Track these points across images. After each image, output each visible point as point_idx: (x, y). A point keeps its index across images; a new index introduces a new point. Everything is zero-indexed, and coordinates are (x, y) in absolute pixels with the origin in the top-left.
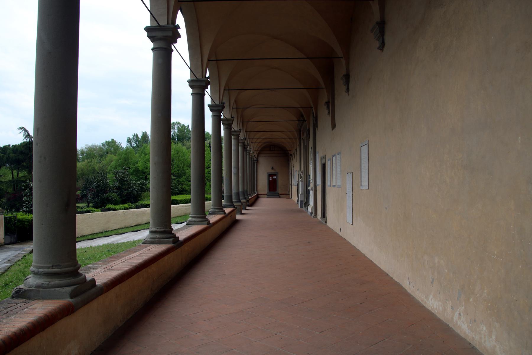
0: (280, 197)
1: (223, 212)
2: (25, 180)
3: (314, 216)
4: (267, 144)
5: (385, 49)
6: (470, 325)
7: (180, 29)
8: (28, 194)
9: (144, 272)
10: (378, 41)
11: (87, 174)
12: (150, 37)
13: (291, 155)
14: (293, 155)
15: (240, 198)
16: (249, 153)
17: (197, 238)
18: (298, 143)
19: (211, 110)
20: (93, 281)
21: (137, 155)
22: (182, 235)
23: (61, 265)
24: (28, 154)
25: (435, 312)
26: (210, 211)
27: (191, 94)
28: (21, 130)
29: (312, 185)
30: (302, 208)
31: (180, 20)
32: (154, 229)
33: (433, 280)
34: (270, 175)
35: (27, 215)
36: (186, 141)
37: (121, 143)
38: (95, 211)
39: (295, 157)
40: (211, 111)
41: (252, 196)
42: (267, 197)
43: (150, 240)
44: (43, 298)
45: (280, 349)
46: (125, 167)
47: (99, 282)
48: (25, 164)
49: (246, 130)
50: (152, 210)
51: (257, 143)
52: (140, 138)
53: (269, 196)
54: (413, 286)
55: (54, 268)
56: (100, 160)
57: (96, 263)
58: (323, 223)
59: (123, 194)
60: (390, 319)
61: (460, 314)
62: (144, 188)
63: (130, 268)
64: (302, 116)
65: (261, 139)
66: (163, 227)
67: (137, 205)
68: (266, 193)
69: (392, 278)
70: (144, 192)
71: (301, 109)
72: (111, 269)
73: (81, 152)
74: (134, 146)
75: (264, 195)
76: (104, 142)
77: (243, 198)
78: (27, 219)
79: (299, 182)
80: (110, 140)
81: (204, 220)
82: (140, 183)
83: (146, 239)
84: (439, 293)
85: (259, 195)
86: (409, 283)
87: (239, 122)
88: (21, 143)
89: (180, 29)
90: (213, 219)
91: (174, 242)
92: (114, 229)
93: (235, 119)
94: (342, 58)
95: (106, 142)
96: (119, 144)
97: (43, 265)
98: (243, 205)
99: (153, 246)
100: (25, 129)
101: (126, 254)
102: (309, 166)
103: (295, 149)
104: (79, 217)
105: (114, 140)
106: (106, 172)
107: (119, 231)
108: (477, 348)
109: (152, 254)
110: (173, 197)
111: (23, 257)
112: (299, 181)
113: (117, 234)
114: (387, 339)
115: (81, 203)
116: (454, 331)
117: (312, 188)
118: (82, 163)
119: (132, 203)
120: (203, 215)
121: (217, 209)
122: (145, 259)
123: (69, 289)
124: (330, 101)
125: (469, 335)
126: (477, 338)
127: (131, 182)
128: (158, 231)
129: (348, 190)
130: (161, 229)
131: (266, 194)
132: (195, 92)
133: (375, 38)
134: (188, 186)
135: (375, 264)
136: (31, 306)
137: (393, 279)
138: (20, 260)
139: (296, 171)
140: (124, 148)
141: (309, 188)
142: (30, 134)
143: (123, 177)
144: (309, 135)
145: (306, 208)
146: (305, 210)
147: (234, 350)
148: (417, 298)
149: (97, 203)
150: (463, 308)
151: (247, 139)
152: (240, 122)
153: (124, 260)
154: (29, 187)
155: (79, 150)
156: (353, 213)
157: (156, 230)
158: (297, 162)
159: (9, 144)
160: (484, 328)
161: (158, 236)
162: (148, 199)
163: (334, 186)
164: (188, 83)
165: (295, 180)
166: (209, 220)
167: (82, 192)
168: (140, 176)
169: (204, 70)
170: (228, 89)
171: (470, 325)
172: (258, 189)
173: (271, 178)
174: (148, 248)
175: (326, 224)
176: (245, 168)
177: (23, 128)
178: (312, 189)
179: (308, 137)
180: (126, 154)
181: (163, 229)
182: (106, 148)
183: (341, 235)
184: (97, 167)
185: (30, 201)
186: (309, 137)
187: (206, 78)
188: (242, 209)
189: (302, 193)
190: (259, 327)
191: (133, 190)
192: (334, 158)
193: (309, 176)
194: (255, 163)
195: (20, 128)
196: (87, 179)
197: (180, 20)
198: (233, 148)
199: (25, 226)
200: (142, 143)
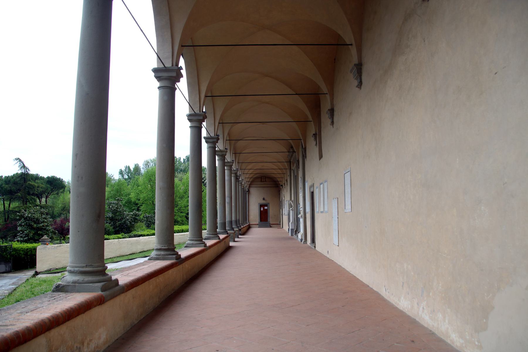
0: (271, 227)
1: (218, 238)
2: (18, 210)
4: (258, 175)
5: (362, 87)
6: (431, 315)
8: (23, 224)
9: (153, 281)
10: (357, 80)
12: (156, 77)
13: (282, 186)
14: (284, 185)
15: (233, 227)
16: (241, 183)
18: (289, 174)
19: (207, 142)
20: (117, 281)
21: (129, 186)
23: (93, 265)
24: (23, 185)
25: (406, 311)
26: (206, 237)
27: (190, 127)
28: (17, 161)
29: (302, 213)
30: (293, 236)
31: (182, 63)
33: (403, 283)
34: (261, 206)
35: (23, 244)
36: (178, 173)
37: (112, 175)
39: (286, 187)
42: (258, 227)
43: (155, 256)
44: (78, 291)
46: (118, 198)
47: (121, 282)
48: (19, 194)
49: (238, 161)
51: (249, 179)
52: (132, 170)
53: (260, 226)
54: (389, 292)
55: (88, 267)
58: (312, 248)
59: (116, 225)
61: (423, 308)
62: (137, 219)
64: (292, 147)
65: (253, 170)
66: (167, 245)
67: (130, 236)
68: (258, 223)
69: (372, 289)
70: (137, 223)
74: (126, 178)
75: (255, 225)
78: (22, 248)
79: (289, 211)
82: (133, 214)
84: (408, 294)
86: (386, 290)
87: (232, 154)
88: (14, 175)
90: (209, 243)
93: (228, 151)
94: (327, 94)
96: (111, 176)
97: (78, 265)
98: (236, 233)
99: (158, 261)
100: (20, 161)
102: (299, 194)
103: (286, 179)
107: (115, 260)
110: (176, 228)
111: (26, 280)
112: (290, 210)
117: (302, 215)
119: (125, 234)
120: (200, 238)
123: (100, 285)
124: (317, 133)
127: (125, 213)
128: (163, 249)
129: (334, 214)
131: (257, 224)
134: (180, 217)
135: (358, 279)
136: (71, 296)
138: (24, 283)
139: (287, 201)
140: (116, 180)
141: (299, 216)
142: (25, 165)
143: (117, 208)
144: (299, 165)
145: (296, 235)
146: (295, 237)
147: (234, 338)
150: (426, 302)
151: (239, 170)
152: (233, 153)
154: (24, 217)
157: (160, 247)
158: (288, 192)
159: (2, 175)
160: (441, 315)
162: (141, 230)
163: (322, 212)
164: (187, 117)
165: (285, 210)
168: (132, 207)
169: (202, 106)
170: (222, 123)
171: (431, 315)
172: (250, 219)
173: (262, 208)
175: (315, 249)
176: (237, 198)
177: (18, 159)
178: (302, 217)
179: (298, 167)
180: (118, 186)
183: (328, 257)
185: (24, 231)
186: (299, 168)
189: (292, 222)
191: (126, 221)
192: (322, 186)
193: (299, 205)
194: (246, 193)
195: (16, 159)
197: (182, 63)
198: (227, 178)
199: (21, 255)
200: (134, 175)
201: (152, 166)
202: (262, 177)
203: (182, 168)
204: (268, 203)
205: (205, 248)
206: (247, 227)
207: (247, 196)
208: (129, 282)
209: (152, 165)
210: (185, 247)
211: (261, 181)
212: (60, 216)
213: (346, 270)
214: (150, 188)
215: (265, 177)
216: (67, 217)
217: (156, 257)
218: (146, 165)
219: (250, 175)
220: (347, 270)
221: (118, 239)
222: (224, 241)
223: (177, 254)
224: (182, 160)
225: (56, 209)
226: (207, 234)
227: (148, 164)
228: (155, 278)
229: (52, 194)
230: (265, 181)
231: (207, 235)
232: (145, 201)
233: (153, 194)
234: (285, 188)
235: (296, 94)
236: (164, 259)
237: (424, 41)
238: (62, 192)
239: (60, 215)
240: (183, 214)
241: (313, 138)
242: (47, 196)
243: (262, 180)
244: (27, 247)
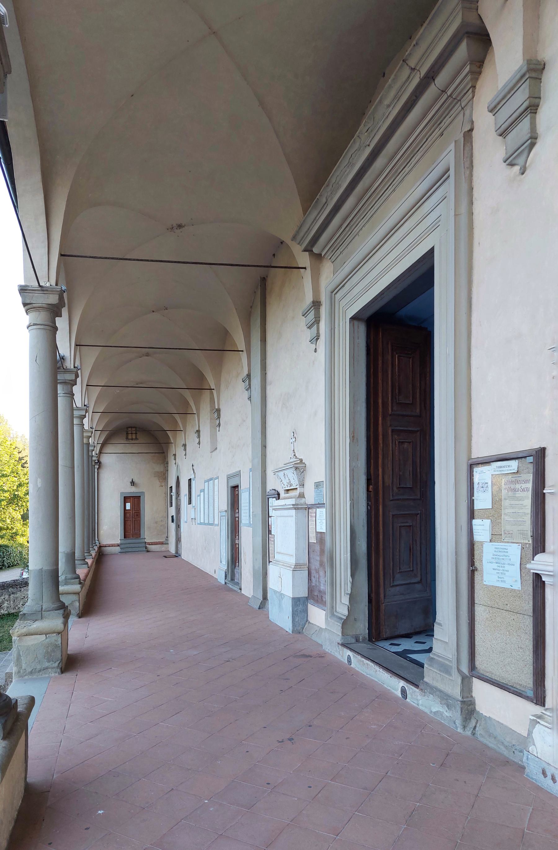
68: (119, 542)
202: (130, 429)
243: (130, 437)
244: (48, 647)
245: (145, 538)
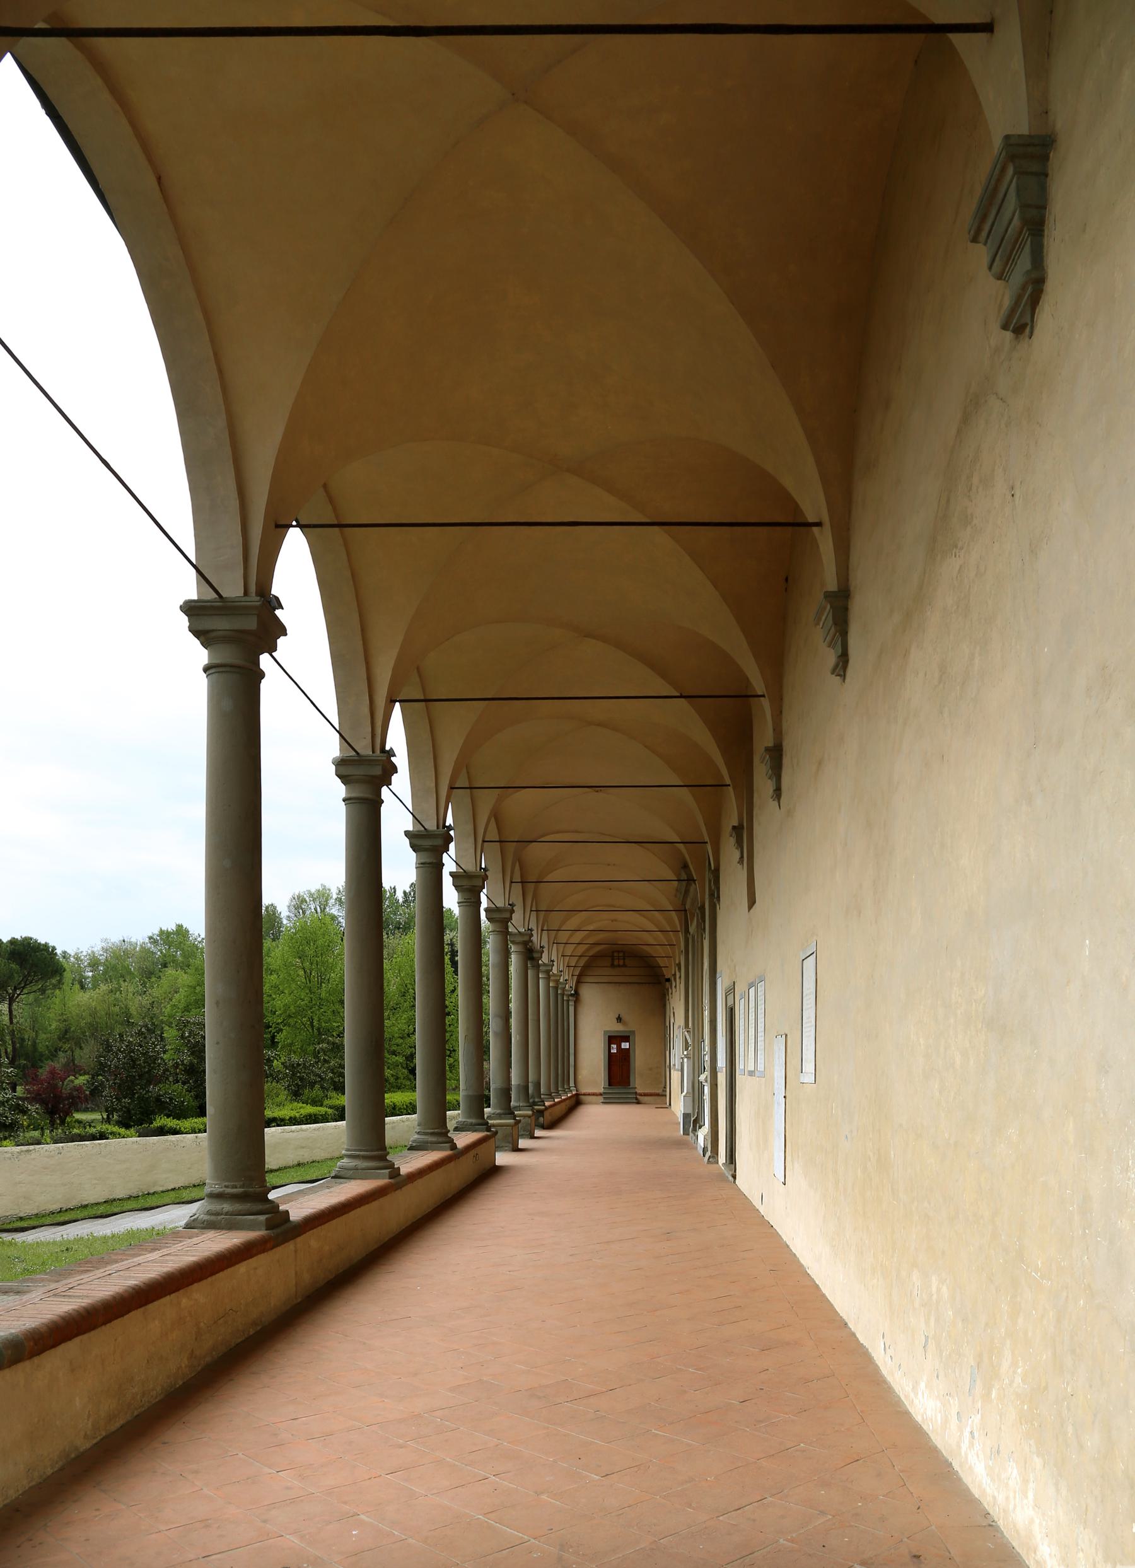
3: (710, 1157)
7: (283, 609)
9: (165, 1306)
11: (106, 1027)
12: (196, 632)
16: (548, 972)
17: (353, 1214)
22: (298, 1211)
26: (413, 1142)
30: (689, 1135)
32: (217, 1189)
33: (927, 1338)
34: (612, 1039)
36: (387, 934)
38: (119, 1134)
40: (414, 851)
41: (556, 1100)
43: (206, 1217)
45: (480, 1517)
50: (210, 1138)
51: (577, 957)
56: (144, 985)
57: (32, 1279)
60: (802, 1445)
63: (118, 1293)
64: (685, 866)
66: (242, 1183)
68: (602, 1091)
69: (854, 1335)
71: (681, 844)
72: (64, 1294)
73: (91, 960)
76: (157, 932)
77: (525, 1104)
80: (171, 927)
81: (381, 1164)
83: (195, 1214)
85: (582, 1097)
89: (283, 609)
91: (269, 1226)
92: (170, 1188)
94: (763, 696)
95: (162, 932)
99: (211, 1234)
101: (128, 1255)
104: (70, 1152)
105: (182, 926)
106: (162, 1022)
108: (999, 1527)
109: (194, 1256)
110: (391, 1098)
113: (178, 1201)
114: (771, 1499)
115: (91, 1111)
116: (960, 1479)
118: (93, 993)
120: (377, 1150)
121: (432, 1134)
122: (169, 1269)
124: (745, 824)
125: (988, 1491)
126: (1001, 1498)
128: (228, 1194)
130: (236, 1188)
131: (601, 1094)
132: (353, 795)
133: (824, 641)
135: (824, 1295)
137: (855, 1336)
147: (362, 1517)
148: (897, 1388)
149: (129, 1111)
150: (979, 1416)
153: (110, 1272)
155: (85, 953)
156: (785, 1152)
157: (222, 1189)
160: (1015, 1471)
161: (227, 1207)
163: (751, 1073)
164: (333, 768)
165: (677, 1054)
166: (396, 1166)
167: (93, 1078)
172: (580, 1077)
173: (614, 1046)
174: (195, 1241)
175: (734, 1182)
181: (240, 1188)
182: (161, 951)
184: (136, 1004)
187: (382, 754)
188: (519, 1136)
190: (448, 1459)
196: (108, 1041)
201: (313, 910)
203: (401, 918)
204: (630, 1031)
205: (390, 1180)
206: (573, 1100)
207: (572, 1009)
208: (46, 1325)
209: (313, 908)
210: (333, 1177)
211: (613, 966)
212: (56, 1057)
213: (799, 1261)
214: (304, 980)
215: (624, 952)
216: (73, 1061)
217: (208, 1221)
218: (297, 907)
219: (575, 948)
220: (802, 1261)
221: (196, 1135)
222: (473, 1152)
223: (391, 1166)
224: (400, 896)
225: (42, 1036)
226: (418, 1133)
227: (303, 907)
228: (173, 1295)
229: (25, 991)
230: (624, 966)
231: (416, 1136)
232: (290, 1016)
233: (312, 996)
234: (676, 987)
235: (681, 697)
236: (231, 1226)
237: (1013, 495)
238: (55, 987)
239: (54, 1053)
240: (397, 1058)
241: (731, 838)
242: (13, 996)
243: (616, 963)
245: (636, 1088)
